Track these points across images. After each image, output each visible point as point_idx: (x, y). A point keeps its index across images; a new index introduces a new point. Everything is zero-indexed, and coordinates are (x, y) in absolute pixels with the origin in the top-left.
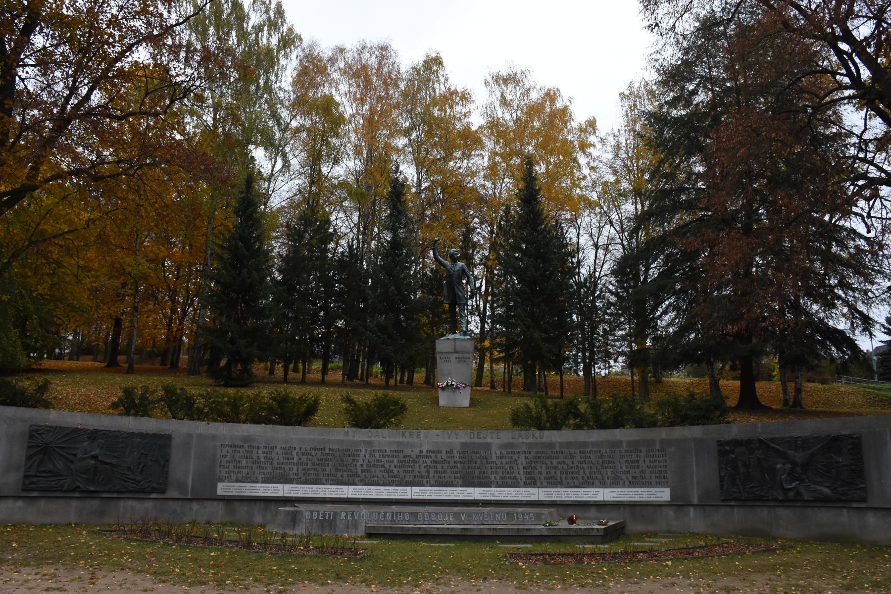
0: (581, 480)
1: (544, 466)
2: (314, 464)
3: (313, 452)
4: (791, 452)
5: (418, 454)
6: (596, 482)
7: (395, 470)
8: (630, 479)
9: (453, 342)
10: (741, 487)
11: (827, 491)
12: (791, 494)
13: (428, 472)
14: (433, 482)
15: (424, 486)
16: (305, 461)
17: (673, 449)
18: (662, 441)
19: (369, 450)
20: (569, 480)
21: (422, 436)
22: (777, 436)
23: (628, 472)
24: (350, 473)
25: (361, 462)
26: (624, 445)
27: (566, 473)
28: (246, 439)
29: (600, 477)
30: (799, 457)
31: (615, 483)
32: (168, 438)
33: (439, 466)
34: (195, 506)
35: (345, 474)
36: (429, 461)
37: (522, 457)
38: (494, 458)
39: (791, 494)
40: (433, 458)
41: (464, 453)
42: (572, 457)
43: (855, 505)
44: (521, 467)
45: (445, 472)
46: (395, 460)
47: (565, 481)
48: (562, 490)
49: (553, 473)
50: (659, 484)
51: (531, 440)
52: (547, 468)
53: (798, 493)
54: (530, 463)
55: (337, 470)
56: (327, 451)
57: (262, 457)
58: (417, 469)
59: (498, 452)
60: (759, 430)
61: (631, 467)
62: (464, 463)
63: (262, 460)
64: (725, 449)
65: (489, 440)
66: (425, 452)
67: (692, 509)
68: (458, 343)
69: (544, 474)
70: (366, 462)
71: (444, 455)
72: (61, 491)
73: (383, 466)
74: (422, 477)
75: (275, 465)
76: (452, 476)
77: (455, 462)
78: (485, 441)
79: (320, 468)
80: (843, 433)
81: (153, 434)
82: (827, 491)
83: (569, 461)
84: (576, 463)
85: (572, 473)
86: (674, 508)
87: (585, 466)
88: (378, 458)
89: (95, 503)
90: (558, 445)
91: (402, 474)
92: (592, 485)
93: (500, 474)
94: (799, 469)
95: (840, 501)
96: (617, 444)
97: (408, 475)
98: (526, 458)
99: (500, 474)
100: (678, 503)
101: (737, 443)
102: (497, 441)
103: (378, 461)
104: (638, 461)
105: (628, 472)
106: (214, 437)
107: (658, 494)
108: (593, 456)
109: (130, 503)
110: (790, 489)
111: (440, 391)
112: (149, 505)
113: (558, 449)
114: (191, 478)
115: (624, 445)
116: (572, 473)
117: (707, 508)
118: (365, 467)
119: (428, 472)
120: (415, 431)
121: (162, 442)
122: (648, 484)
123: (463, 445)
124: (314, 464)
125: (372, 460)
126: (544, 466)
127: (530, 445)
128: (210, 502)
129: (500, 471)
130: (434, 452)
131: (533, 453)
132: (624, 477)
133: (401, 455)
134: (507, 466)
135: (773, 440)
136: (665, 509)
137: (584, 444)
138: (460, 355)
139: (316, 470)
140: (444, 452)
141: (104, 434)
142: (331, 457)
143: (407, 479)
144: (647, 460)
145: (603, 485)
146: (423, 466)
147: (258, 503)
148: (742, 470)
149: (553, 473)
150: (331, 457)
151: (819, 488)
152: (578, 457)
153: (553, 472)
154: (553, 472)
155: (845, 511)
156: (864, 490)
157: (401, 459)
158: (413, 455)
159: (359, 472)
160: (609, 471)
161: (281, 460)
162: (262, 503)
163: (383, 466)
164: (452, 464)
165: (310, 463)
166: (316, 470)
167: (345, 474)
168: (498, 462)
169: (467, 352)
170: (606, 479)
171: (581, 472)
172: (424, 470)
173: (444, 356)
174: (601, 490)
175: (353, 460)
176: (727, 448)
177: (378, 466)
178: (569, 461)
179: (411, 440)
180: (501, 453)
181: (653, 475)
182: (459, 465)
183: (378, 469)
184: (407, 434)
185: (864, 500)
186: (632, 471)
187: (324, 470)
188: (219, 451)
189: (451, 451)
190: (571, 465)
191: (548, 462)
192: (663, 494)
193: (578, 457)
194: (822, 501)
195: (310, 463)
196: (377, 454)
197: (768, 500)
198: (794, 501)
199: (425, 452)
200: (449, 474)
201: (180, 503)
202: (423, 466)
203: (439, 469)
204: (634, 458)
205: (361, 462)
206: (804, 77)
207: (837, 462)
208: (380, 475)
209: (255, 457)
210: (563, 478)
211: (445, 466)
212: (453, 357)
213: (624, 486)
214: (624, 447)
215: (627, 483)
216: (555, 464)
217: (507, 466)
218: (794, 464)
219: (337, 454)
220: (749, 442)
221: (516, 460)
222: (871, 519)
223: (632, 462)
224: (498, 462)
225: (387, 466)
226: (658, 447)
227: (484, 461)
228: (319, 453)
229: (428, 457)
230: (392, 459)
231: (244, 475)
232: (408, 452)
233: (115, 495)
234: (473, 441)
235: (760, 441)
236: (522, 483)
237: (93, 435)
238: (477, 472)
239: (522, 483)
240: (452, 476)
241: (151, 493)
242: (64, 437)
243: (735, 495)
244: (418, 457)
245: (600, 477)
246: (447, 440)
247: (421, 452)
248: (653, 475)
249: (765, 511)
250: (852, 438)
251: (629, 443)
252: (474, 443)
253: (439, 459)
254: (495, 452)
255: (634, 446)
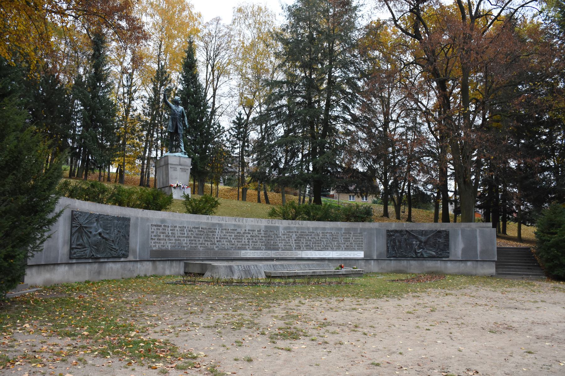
0: (322, 247)
1: (305, 239)
2: (194, 237)
3: (194, 230)
4: (420, 237)
5: (244, 232)
6: (330, 248)
7: (233, 241)
8: (345, 247)
9: (178, 158)
10: (397, 251)
11: (434, 253)
12: (419, 255)
13: (249, 242)
14: (251, 248)
15: (247, 250)
16: (190, 235)
17: (366, 233)
18: (361, 229)
19: (220, 229)
20: (317, 247)
21: (244, 221)
22: (413, 229)
23: (345, 243)
24: (211, 243)
25: (217, 236)
26: (343, 230)
27: (315, 243)
28: (163, 221)
29: (331, 245)
30: (423, 239)
31: (338, 248)
32: (128, 220)
33: (254, 238)
34: (139, 265)
35: (209, 243)
36: (249, 235)
37: (294, 234)
38: (281, 235)
39: (419, 255)
40: (251, 234)
41: (266, 231)
42: (318, 235)
43: (444, 259)
44: (293, 240)
45: (257, 242)
46: (233, 235)
47: (314, 248)
48: (313, 252)
49: (309, 244)
50: (359, 249)
51: (297, 225)
52: (306, 240)
53: (422, 254)
54: (298, 238)
55: (205, 241)
56: (200, 229)
57: (170, 232)
58: (243, 241)
59: (283, 231)
60: (405, 226)
61: (346, 241)
62: (266, 237)
63: (170, 234)
64: (390, 234)
65: (277, 225)
66: (247, 230)
67: (372, 262)
68: (181, 159)
69: (304, 244)
70: (219, 236)
71: (256, 232)
72: (86, 258)
73: (227, 238)
74: (246, 245)
75: (176, 238)
76: (260, 244)
77: (262, 237)
78: (275, 225)
79: (197, 239)
80: (442, 229)
81: (118, 217)
82: (434, 253)
83: (317, 237)
84: (320, 238)
85: (318, 243)
86: (364, 261)
87: (324, 240)
88: (225, 234)
89: (96, 266)
90: (311, 229)
91: (236, 243)
92: (327, 250)
93: (284, 244)
94: (423, 244)
95: (438, 257)
96: (340, 229)
97: (239, 244)
98: (296, 235)
99: (284, 244)
100: (367, 259)
101: (396, 231)
102: (281, 225)
103: (224, 235)
104: (349, 238)
105: (345, 243)
106: (148, 219)
107: (358, 254)
108: (328, 235)
109: (111, 265)
110: (419, 253)
111: (173, 189)
112: (118, 265)
113: (311, 231)
114: (138, 247)
115: (343, 230)
116: (318, 243)
117: (379, 261)
118: (218, 239)
119: (249, 242)
120: (241, 218)
121: (125, 221)
122: (354, 250)
123: (266, 227)
124: (194, 237)
125: (222, 235)
126: (305, 239)
127: (298, 228)
128: (146, 262)
129: (283, 242)
130: (252, 231)
131: (299, 233)
132: (342, 246)
133: (236, 232)
134: (287, 239)
135: (412, 231)
136: (360, 261)
137: (324, 229)
138: (183, 167)
139: (195, 241)
140: (256, 231)
141: (103, 217)
142: (202, 233)
143: (239, 246)
144: (354, 238)
145: (332, 249)
146: (246, 239)
147: (167, 262)
148: (398, 244)
149: (309, 244)
150: (202, 233)
151: (431, 252)
152: (321, 235)
153: (309, 242)
154: (309, 242)
155: (439, 262)
156: (449, 253)
157: (236, 234)
158: (242, 232)
159: (216, 242)
160: (336, 243)
161: (179, 235)
162: (169, 261)
163: (227, 238)
164: (260, 238)
165: (192, 236)
166: (195, 241)
167: (209, 243)
168: (283, 237)
169: (187, 166)
170: (334, 247)
171: (322, 242)
172: (247, 241)
173: (173, 166)
174: (331, 252)
175: (213, 235)
176: (391, 233)
177: (225, 238)
178: (317, 237)
179: (239, 223)
180: (284, 232)
181: (356, 245)
182: (264, 238)
183: (225, 240)
184: (237, 220)
185: (448, 257)
186: (346, 243)
187: (199, 241)
188: (150, 229)
189: (260, 231)
190: (317, 239)
191: (307, 237)
192: (360, 254)
193: (321, 235)
194: (432, 258)
195: (192, 236)
196: (224, 231)
197: (408, 257)
198: (419, 257)
199: (247, 230)
200: (259, 243)
201: (132, 263)
202: (246, 239)
203: (254, 240)
204: (348, 236)
205: (217, 236)
206: (453, 86)
207: (439, 242)
208: (226, 243)
209: (167, 233)
210: (314, 246)
211: (257, 238)
212: (179, 168)
213: (342, 250)
214: (343, 231)
215: (344, 249)
216: (310, 239)
217: (287, 239)
218: (421, 242)
219: (205, 231)
220: (401, 231)
221: (291, 236)
222: (449, 264)
223: (347, 238)
224: (283, 237)
225: (229, 238)
226: (359, 232)
227: (276, 236)
228: (197, 230)
229: (249, 233)
230: (231, 234)
231: (162, 244)
232: (239, 230)
233: (106, 260)
234: (269, 225)
235: (407, 231)
236: (294, 248)
237: (99, 217)
238: (272, 242)
239: (294, 248)
240: (260, 244)
241: (120, 257)
242: (86, 219)
243: (394, 255)
244: (244, 233)
245: (331, 245)
246: (256, 224)
247: (246, 230)
248: (356, 245)
249: (405, 262)
250: (446, 232)
251: (345, 229)
252: (271, 226)
253: (254, 235)
254: (281, 231)
255: (348, 231)
